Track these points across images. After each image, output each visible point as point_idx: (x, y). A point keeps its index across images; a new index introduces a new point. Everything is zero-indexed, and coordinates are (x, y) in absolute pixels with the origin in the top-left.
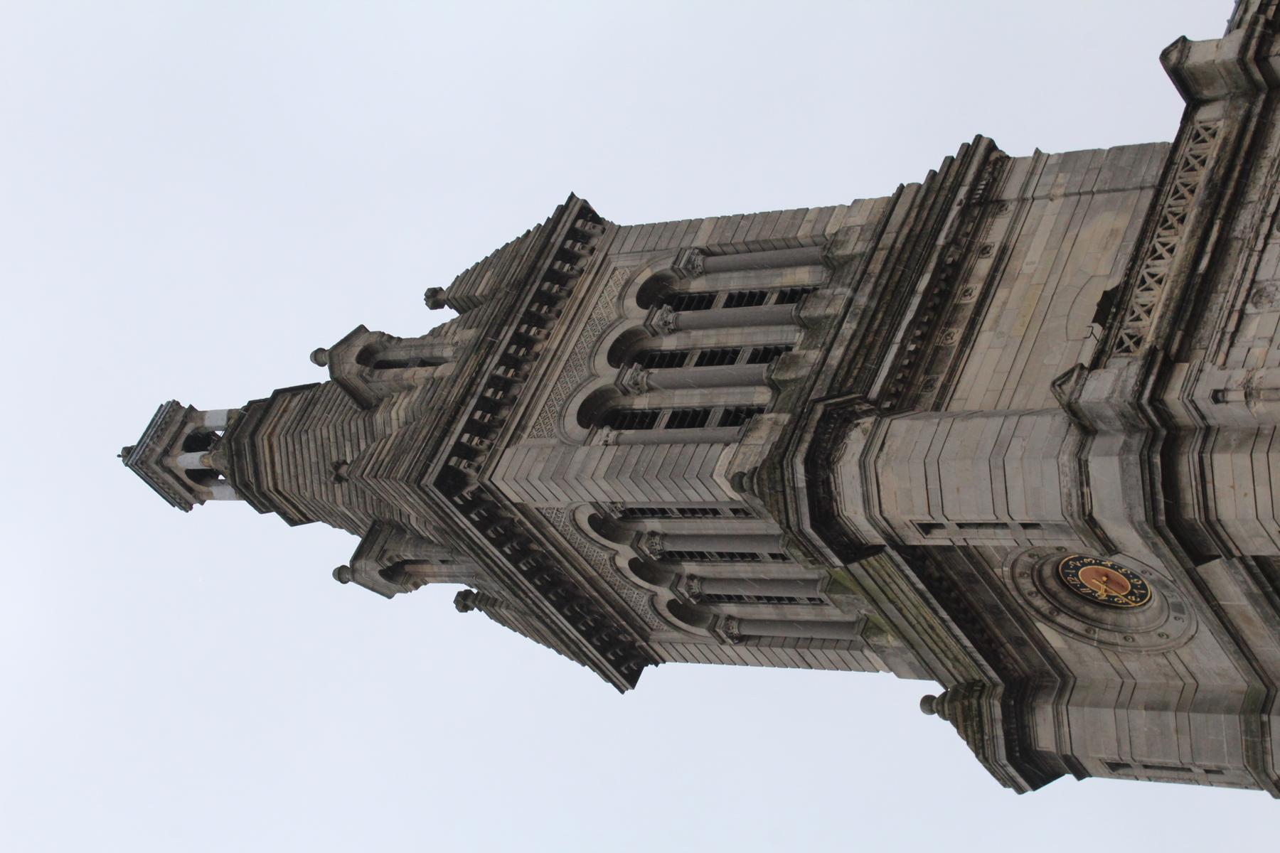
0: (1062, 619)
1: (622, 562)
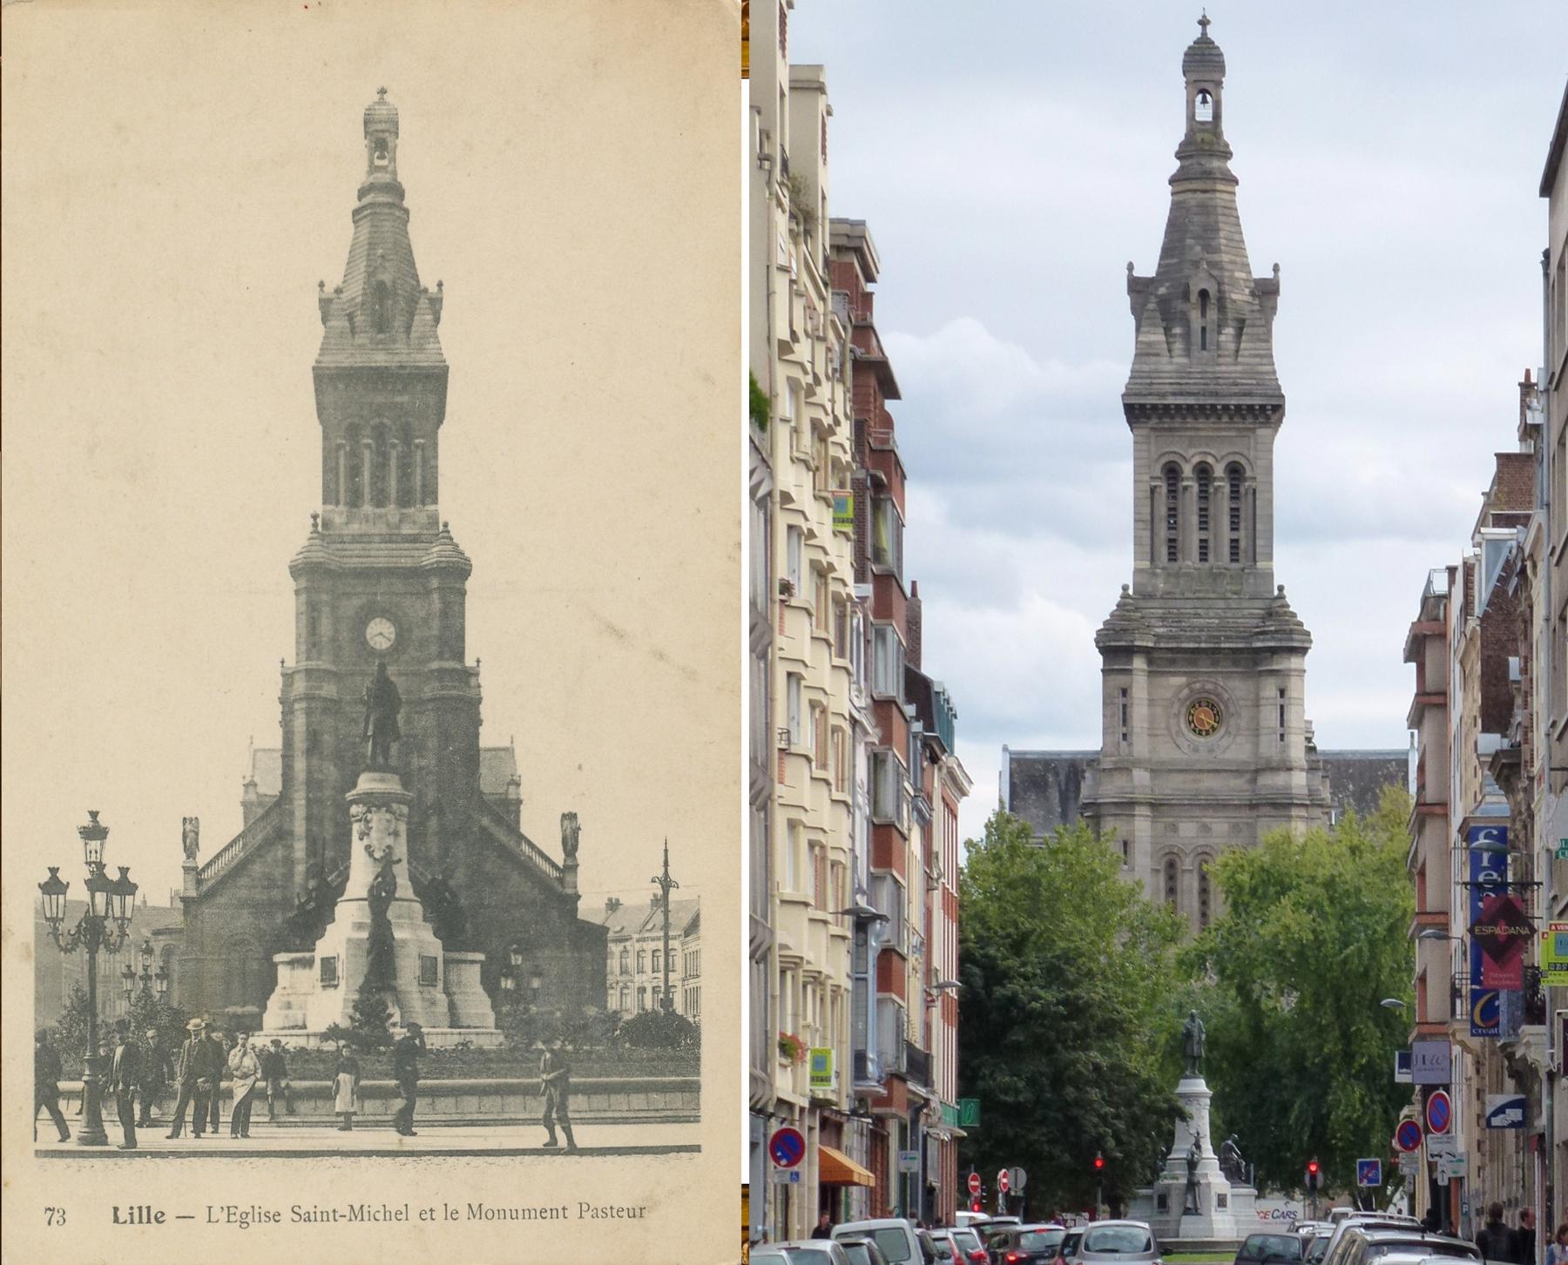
0: (1186, 691)
1: (1210, 460)
